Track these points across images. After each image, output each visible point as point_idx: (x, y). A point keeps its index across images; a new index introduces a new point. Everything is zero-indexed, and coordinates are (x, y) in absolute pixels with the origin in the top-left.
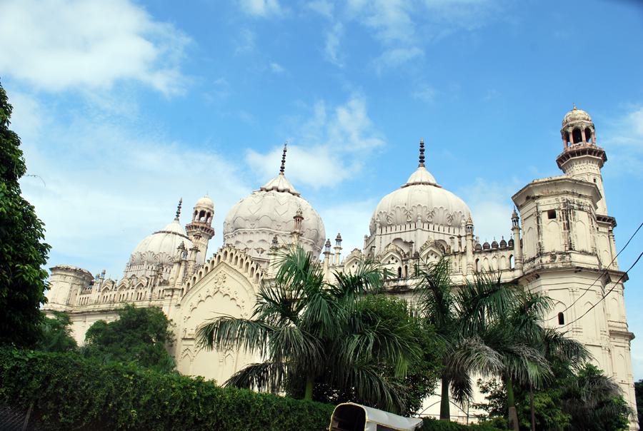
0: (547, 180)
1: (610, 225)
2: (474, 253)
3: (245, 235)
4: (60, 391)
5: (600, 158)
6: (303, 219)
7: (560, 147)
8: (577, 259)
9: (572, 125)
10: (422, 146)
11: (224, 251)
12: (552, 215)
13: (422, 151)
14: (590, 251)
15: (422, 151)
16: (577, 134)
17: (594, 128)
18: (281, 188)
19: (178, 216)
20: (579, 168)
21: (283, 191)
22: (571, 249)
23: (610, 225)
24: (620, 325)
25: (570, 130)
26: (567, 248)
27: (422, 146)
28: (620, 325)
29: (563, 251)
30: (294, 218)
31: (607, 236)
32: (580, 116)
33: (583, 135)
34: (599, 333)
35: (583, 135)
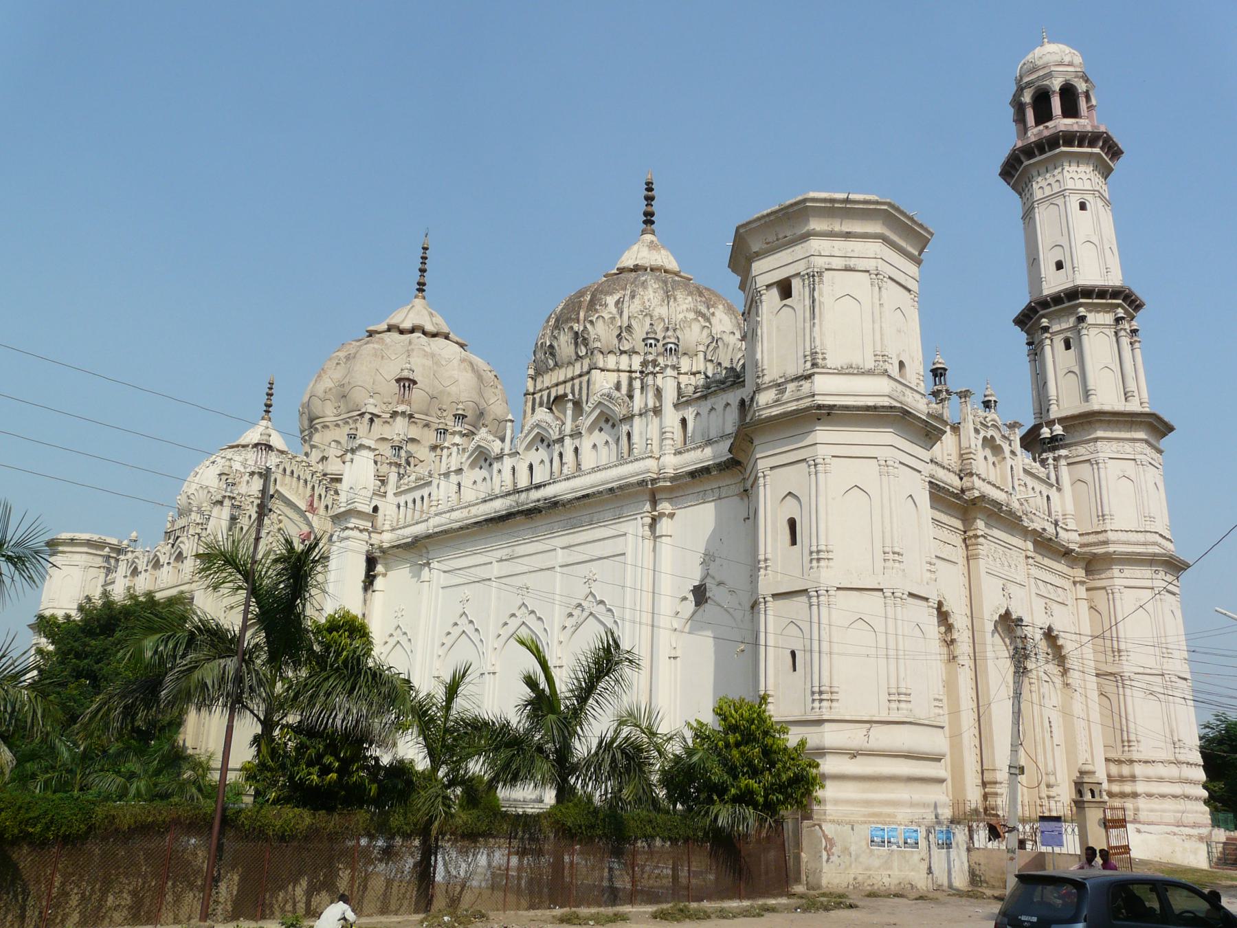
0: (777, 207)
1: (1119, 305)
2: (676, 406)
3: (327, 431)
4: (243, 753)
5: (1097, 150)
6: (415, 383)
7: (1008, 139)
8: (827, 388)
9: (1029, 84)
10: (650, 189)
11: (281, 468)
12: (785, 289)
13: (649, 199)
14: (870, 364)
15: (649, 199)
16: (1042, 100)
17: (1087, 81)
18: (429, 328)
19: (267, 412)
20: (1076, 176)
21: (434, 335)
22: (814, 365)
23: (1119, 305)
24: (1141, 537)
25: (1027, 98)
26: (809, 365)
27: (650, 189)
28: (1141, 537)
29: (800, 372)
30: (398, 381)
31: (1111, 332)
32: (1057, 58)
33: (1056, 103)
34: (879, 556)
35: (1056, 103)
